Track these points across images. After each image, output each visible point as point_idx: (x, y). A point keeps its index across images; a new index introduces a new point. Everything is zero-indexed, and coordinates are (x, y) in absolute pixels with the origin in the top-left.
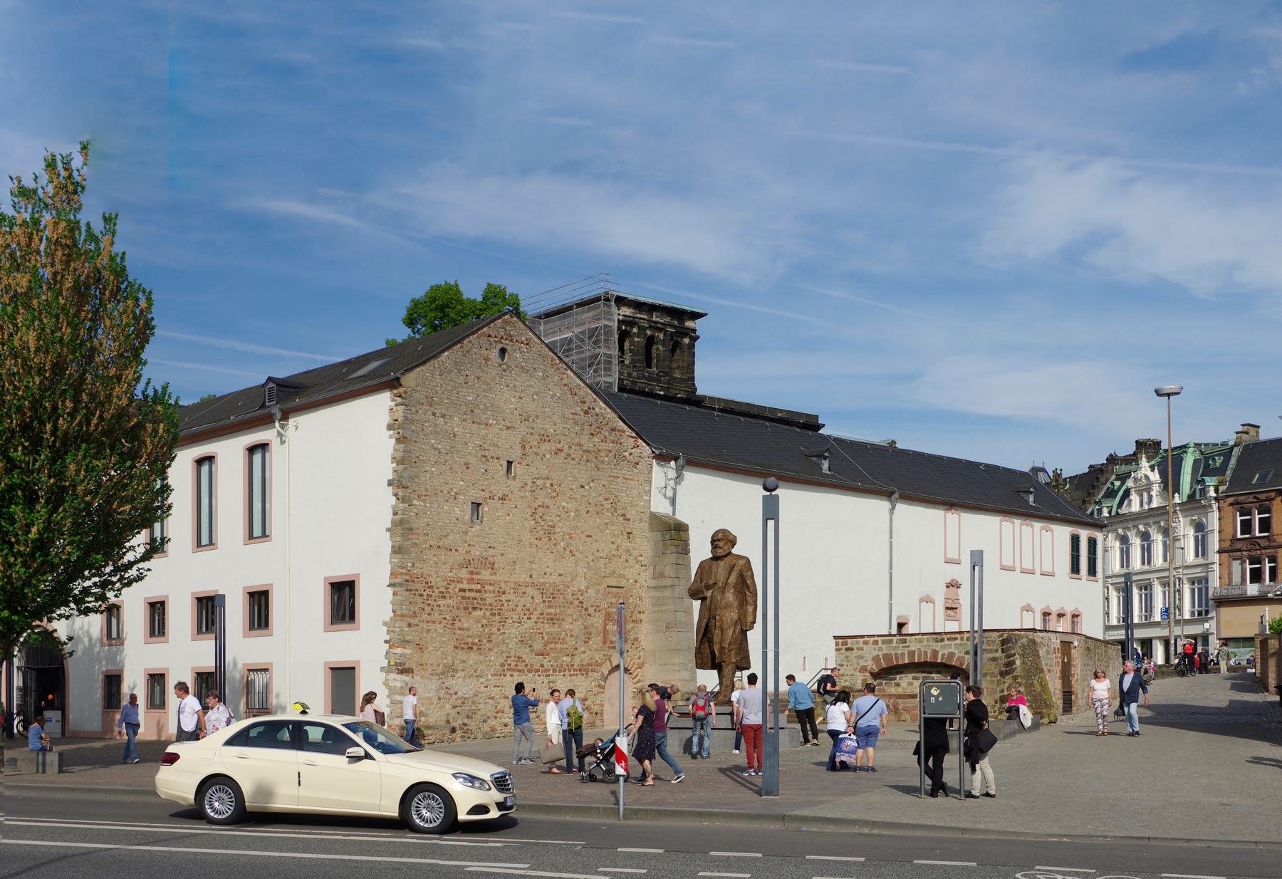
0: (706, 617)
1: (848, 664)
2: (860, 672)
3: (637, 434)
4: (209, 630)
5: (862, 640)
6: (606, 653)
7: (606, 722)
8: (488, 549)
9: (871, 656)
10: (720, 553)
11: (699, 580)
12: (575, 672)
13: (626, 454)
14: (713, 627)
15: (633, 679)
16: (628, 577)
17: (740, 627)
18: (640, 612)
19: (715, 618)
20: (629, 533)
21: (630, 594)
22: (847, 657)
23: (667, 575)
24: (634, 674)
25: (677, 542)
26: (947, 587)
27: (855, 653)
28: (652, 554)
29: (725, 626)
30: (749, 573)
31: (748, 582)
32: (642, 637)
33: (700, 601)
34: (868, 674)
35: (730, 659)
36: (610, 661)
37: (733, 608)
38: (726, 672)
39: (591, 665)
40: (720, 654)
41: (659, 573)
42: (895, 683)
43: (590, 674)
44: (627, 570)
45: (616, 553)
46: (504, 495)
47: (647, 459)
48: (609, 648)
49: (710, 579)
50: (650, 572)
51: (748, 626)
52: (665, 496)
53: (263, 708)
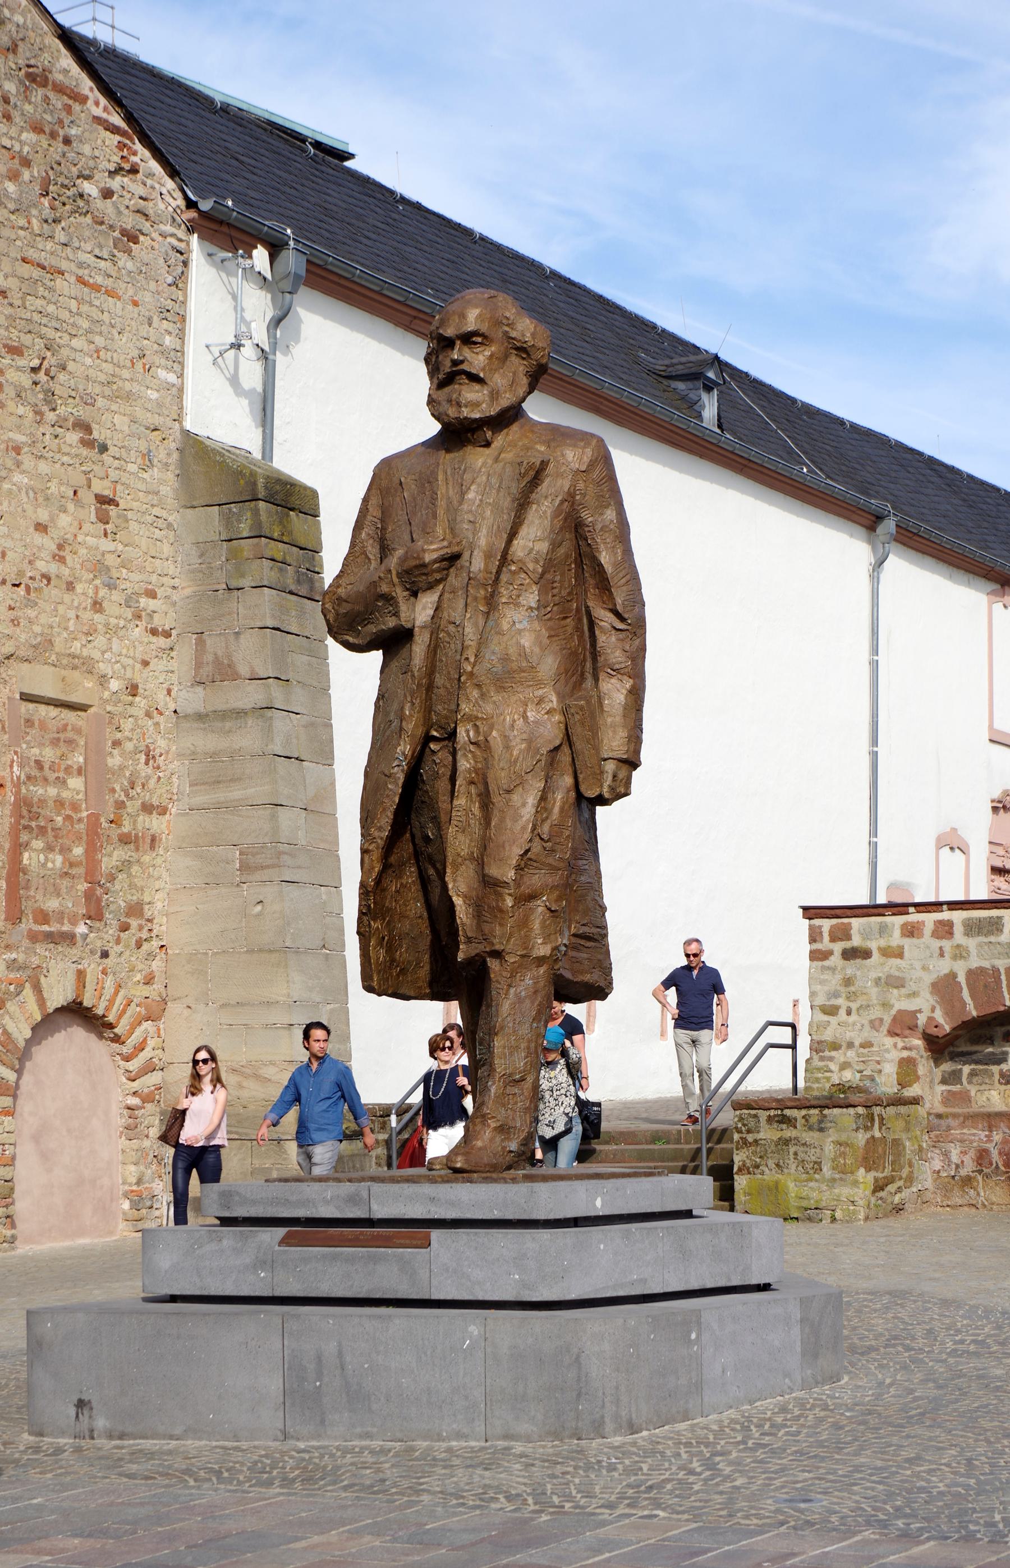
0: (409, 726)
1: (854, 1006)
2: (892, 1033)
3: (129, 118)
5: (899, 920)
6: (21, 957)
7: (23, 1227)
9: (929, 979)
10: (476, 405)
11: (373, 550)
13: (90, 188)
14: (443, 785)
15: (127, 1059)
16: (103, 667)
17: (568, 780)
18: (147, 808)
19: (452, 735)
20: (104, 501)
21: (110, 735)
22: (848, 982)
23: (244, 670)
24: (132, 1041)
25: (278, 550)
26: (995, 809)
27: (876, 967)
28: (188, 592)
29: (500, 776)
30: (610, 514)
31: (605, 558)
32: (158, 904)
33: (377, 656)
34: (918, 1042)
35: (526, 943)
36: (37, 989)
37: (539, 684)
38: (505, 1007)
40: (478, 915)
41: (217, 659)
42: (1002, 1075)
44: (100, 641)
45: (53, 568)
47: (168, 228)
48: (34, 937)
49: (427, 531)
50: (185, 651)
51: (608, 780)
52: (234, 381)
53: (793, 1047)
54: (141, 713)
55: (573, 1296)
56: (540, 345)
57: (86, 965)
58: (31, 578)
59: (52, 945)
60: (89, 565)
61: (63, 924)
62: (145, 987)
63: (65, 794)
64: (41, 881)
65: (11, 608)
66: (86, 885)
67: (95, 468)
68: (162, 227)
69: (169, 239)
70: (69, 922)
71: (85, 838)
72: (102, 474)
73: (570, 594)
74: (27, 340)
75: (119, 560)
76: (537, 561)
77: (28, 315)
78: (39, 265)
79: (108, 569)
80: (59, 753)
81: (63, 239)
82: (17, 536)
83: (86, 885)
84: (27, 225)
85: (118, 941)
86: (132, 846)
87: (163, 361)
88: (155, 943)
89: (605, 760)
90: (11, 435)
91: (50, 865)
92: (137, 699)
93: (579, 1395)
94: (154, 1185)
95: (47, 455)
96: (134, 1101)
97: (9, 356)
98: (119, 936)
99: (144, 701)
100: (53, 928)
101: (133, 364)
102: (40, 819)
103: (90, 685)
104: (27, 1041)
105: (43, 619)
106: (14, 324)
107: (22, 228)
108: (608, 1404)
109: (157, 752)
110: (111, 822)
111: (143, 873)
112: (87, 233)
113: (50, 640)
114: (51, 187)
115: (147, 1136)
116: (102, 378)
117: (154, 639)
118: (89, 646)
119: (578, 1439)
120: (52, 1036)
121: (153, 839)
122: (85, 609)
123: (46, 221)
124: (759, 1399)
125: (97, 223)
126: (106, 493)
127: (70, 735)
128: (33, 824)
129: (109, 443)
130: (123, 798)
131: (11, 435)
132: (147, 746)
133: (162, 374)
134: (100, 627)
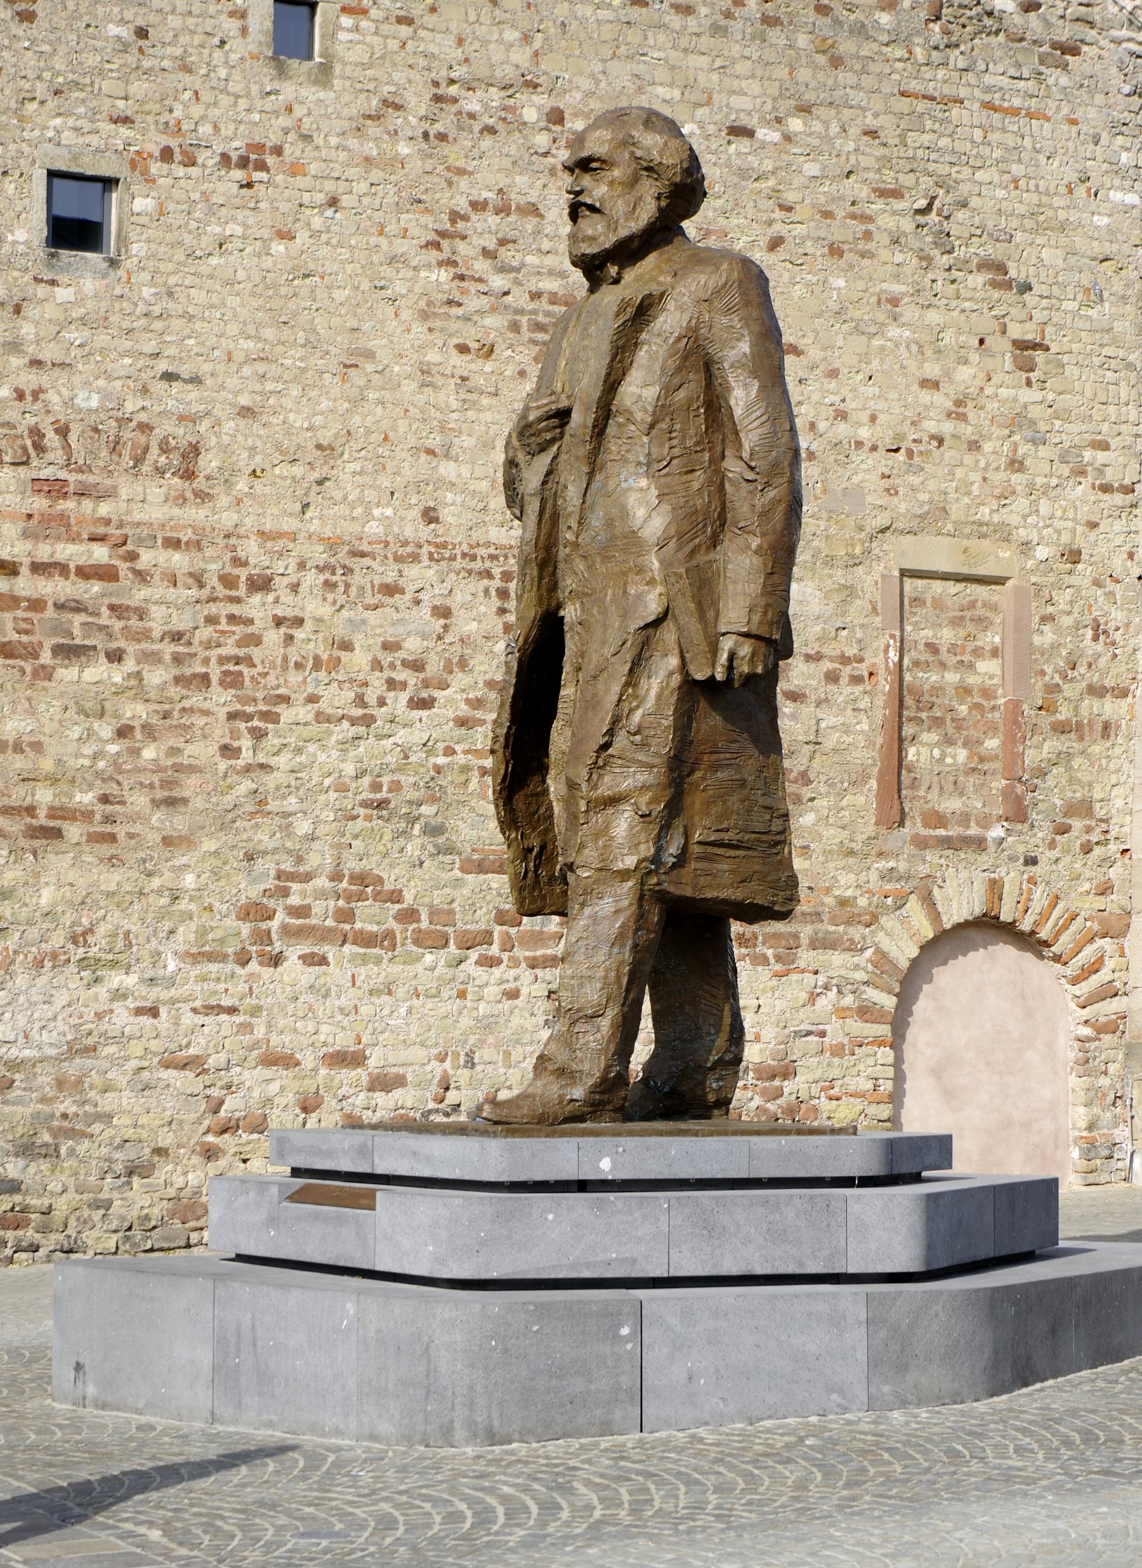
6: (902, 866)
17: (674, 661)
18: (1097, 691)
36: (929, 901)
43: (805, 957)
45: (948, 428)
46: (260, 148)
48: (921, 843)
54: (1087, 582)
55: (495, 1275)
56: (671, 162)
57: (1003, 874)
58: (915, 441)
59: (950, 852)
60: (1001, 420)
61: (968, 827)
62: (1097, 898)
63: (971, 680)
64: (936, 779)
65: (884, 476)
66: (1004, 782)
67: (1013, 311)
68: (1115, 33)
69: (1125, 45)
70: (978, 824)
71: (1001, 728)
72: (1024, 317)
73: (697, 443)
74: (907, 180)
75: (1050, 410)
76: (645, 411)
77: (910, 153)
78: (925, 97)
79: (1033, 423)
80: (962, 633)
81: (961, 64)
82: (894, 395)
83: (1004, 782)
84: (907, 56)
85: (1052, 845)
86: (1073, 735)
87: (1117, 182)
88: (1113, 848)
89: (724, 634)
90: (884, 286)
91: (949, 760)
92: (1080, 566)
93: (428, 1393)
94: (1117, 1132)
95: (938, 303)
96: (1087, 1031)
97: (882, 200)
98: (1053, 840)
99: (1090, 569)
100: (953, 831)
101: (1071, 191)
102: (935, 709)
103: (1007, 554)
104: (914, 962)
105: (932, 485)
106: (888, 165)
107: (899, 60)
108: (458, 1407)
109: (1112, 625)
110: (1040, 708)
111: (1092, 765)
112: (998, 53)
113: (944, 509)
114: (944, 11)
115: (1106, 1073)
116: (1021, 209)
117: (1106, 497)
118: (1005, 510)
119: (427, 1446)
120: (965, 955)
121: (1106, 726)
122: (997, 469)
123: (936, 48)
124: (770, 1417)
125: (1013, 40)
126: (1029, 337)
127: (981, 612)
128: (924, 715)
129: (1033, 281)
130: (1057, 679)
131: (884, 286)
132: (1095, 620)
133: (1116, 196)
134: (1019, 488)
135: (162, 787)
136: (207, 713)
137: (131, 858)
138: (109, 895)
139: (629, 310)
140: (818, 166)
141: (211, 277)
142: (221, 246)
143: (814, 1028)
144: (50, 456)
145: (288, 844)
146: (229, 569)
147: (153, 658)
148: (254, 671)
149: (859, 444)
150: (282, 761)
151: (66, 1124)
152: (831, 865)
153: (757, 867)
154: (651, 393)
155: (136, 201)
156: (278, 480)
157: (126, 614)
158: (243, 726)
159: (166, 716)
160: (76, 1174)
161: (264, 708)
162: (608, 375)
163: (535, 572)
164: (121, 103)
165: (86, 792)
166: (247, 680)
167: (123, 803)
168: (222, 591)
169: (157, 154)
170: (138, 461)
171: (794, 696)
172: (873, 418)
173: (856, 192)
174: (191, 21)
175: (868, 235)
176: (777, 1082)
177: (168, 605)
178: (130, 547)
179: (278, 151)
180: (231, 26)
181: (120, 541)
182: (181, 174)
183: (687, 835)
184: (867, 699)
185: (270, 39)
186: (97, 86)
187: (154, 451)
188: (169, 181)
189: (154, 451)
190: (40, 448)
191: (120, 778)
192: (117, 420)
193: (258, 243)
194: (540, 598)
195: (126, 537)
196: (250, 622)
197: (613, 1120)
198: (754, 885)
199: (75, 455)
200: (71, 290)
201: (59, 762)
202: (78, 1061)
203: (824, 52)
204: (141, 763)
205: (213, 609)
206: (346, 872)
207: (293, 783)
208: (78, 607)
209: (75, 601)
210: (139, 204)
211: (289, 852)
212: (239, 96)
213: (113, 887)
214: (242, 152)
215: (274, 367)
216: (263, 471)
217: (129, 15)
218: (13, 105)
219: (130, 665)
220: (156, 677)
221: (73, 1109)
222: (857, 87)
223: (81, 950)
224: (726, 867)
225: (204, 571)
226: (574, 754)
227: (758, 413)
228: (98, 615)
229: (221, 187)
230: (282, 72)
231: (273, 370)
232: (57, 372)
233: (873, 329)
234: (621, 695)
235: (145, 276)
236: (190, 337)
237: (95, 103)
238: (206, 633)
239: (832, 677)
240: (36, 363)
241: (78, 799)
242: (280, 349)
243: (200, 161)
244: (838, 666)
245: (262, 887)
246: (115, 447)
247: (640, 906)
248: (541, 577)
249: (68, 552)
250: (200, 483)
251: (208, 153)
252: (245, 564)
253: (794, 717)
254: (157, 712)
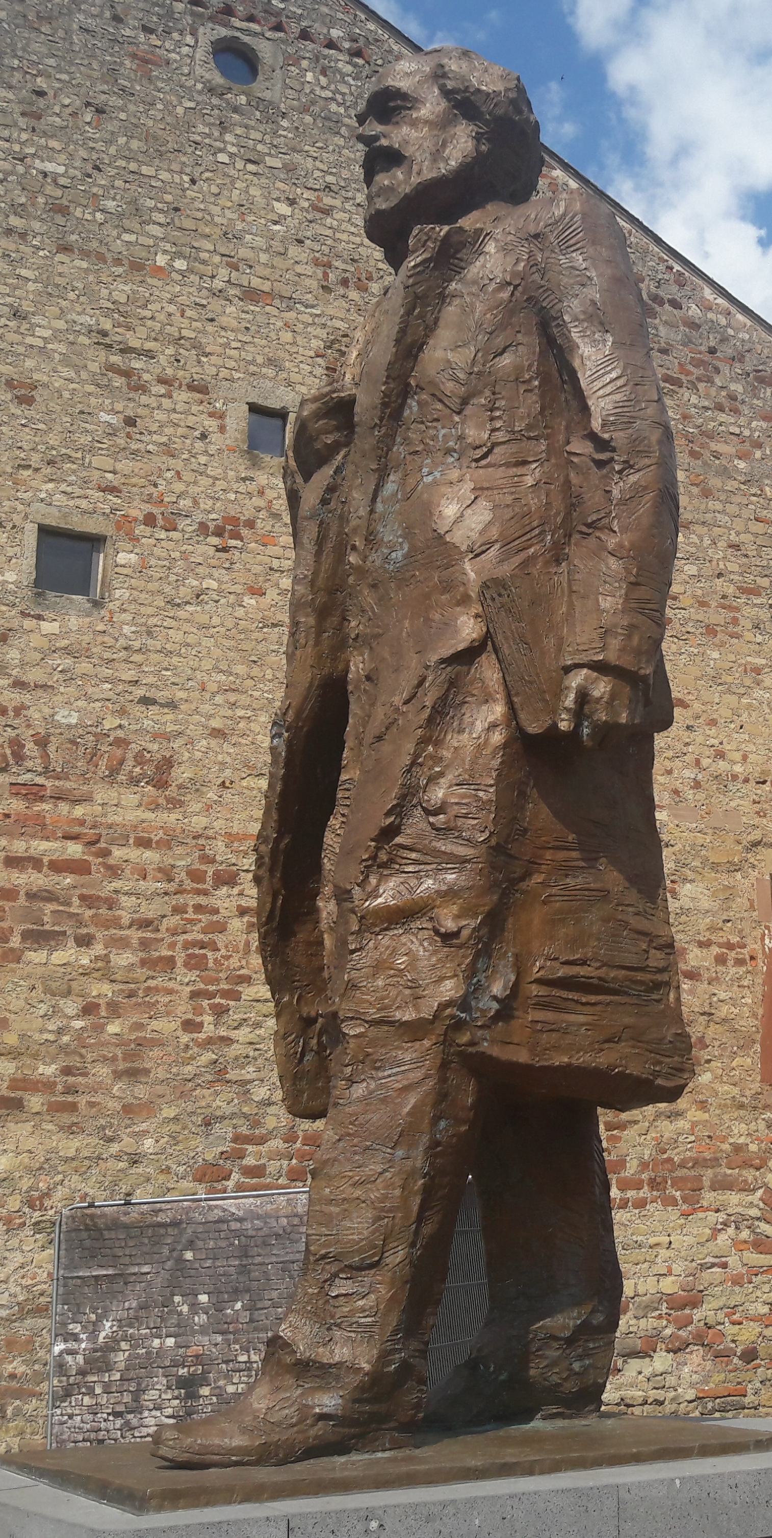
4: (665, 977)
8: (137, 710)
12: (631, 1194)
17: (498, 710)
39: (714, 1162)
43: (708, 1197)
46: (234, 521)
65: (755, 802)
73: (530, 427)
77: (765, 563)
90: (749, 659)
131: (749, 659)
135: (124, 1060)
136: (170, 992)
137: (90, 1125)
138: (67, 1160)
139: (430, 244)
140: (695, 568)
141: (187, 621)
142: (198, 596)
143: (716, 1260)
144: (29, 764)
145: (245, 1110)
146: (197, 866)
147: (122, 943)
148: (218, 955)
149: (735, 777)
150: (243, 1034)
151: (14, 1384)
152: (726, 1117)
153: (628, 1020)
154: (461, 358)
155: (120, 555)
156: (245, 791)
157: (96, 904)
158: (205, 1003)
159: (131, 995)
160: (22, 1433)
161: (226, 987)
162: (403, 332)
163: (312, 621)
164: (109, 476)
165: (49, 1065)
166: (211, 964)
167: (85, 1075)
168: (188, 884)
169: (141, 518)
170: (114, 771)
171: (692, 975)
172: (745, 758)
173: (725, 589)
174: (174, 416)
175: (735, 622)
176: (687, 1311)
177: (138, 895)
178: (102, 845)
179: (251, 524)
180: (212, 424)
181: (94, 838)
182: (162, 537)
183: (520, 969)
184: (749, 977)
185: (245, 437)
186: (87, 460)
187: (130, 762)
188: (152, 541)
189: (130, 762)
190: (19, 757)
191: (83, 1051)
192: (95, 735)
193: (232, 596)
194: (319, 657)
195: (100, 836)
196: (216, 911)
197: (396, 1446)
198: (624, 1048)
199: (53, 764)
200: (56, 624)
201: (22, 1037)
202: (29, 1322)
203: (697, 485)
204: (105, 1037)
205: (181, 899)
206: (300, 1134)
207: (251, 1054)
208: (49, 896)
209: (46, 891)
210: (122, 558)
211: (246, 1116)
212: (217, 479)
213: (71, 1153)
214: (220, 523)
215: (243, 697)
216: (231, 783)
217: (119, 407)
218: (9, 470)
219: (98, 949)
220: (123, 959)
221: (22, 1369)
222: (723, 512)
223: (37, 1214)
224: (582, 1019)
225: (173, 866)
226: (347, 853)
227: (614, 375)
228: (69, 904)
229: (201, 548)
230: (255, 463)
231: (243, 699)
232: (40, 692)
233: (742, 691)
234: (416, 756)
235: (127, 617)
236: (167, 669)
237: (85, 474)
238: (173, 921)
239: (721, 960)
240: (19, 684)
241: (40, 1071)
242: (250, 682)
243: (180, 528)
244: (725, 951)
245: (220, 1149)
246: (93, 756)
247: (443, 1080)
248: (320, 631)
249: (42, 848)
250: (172, 791)
251: (188, 521)
252: (213, 861)
253: (691, 992)
254: (123, 991)
